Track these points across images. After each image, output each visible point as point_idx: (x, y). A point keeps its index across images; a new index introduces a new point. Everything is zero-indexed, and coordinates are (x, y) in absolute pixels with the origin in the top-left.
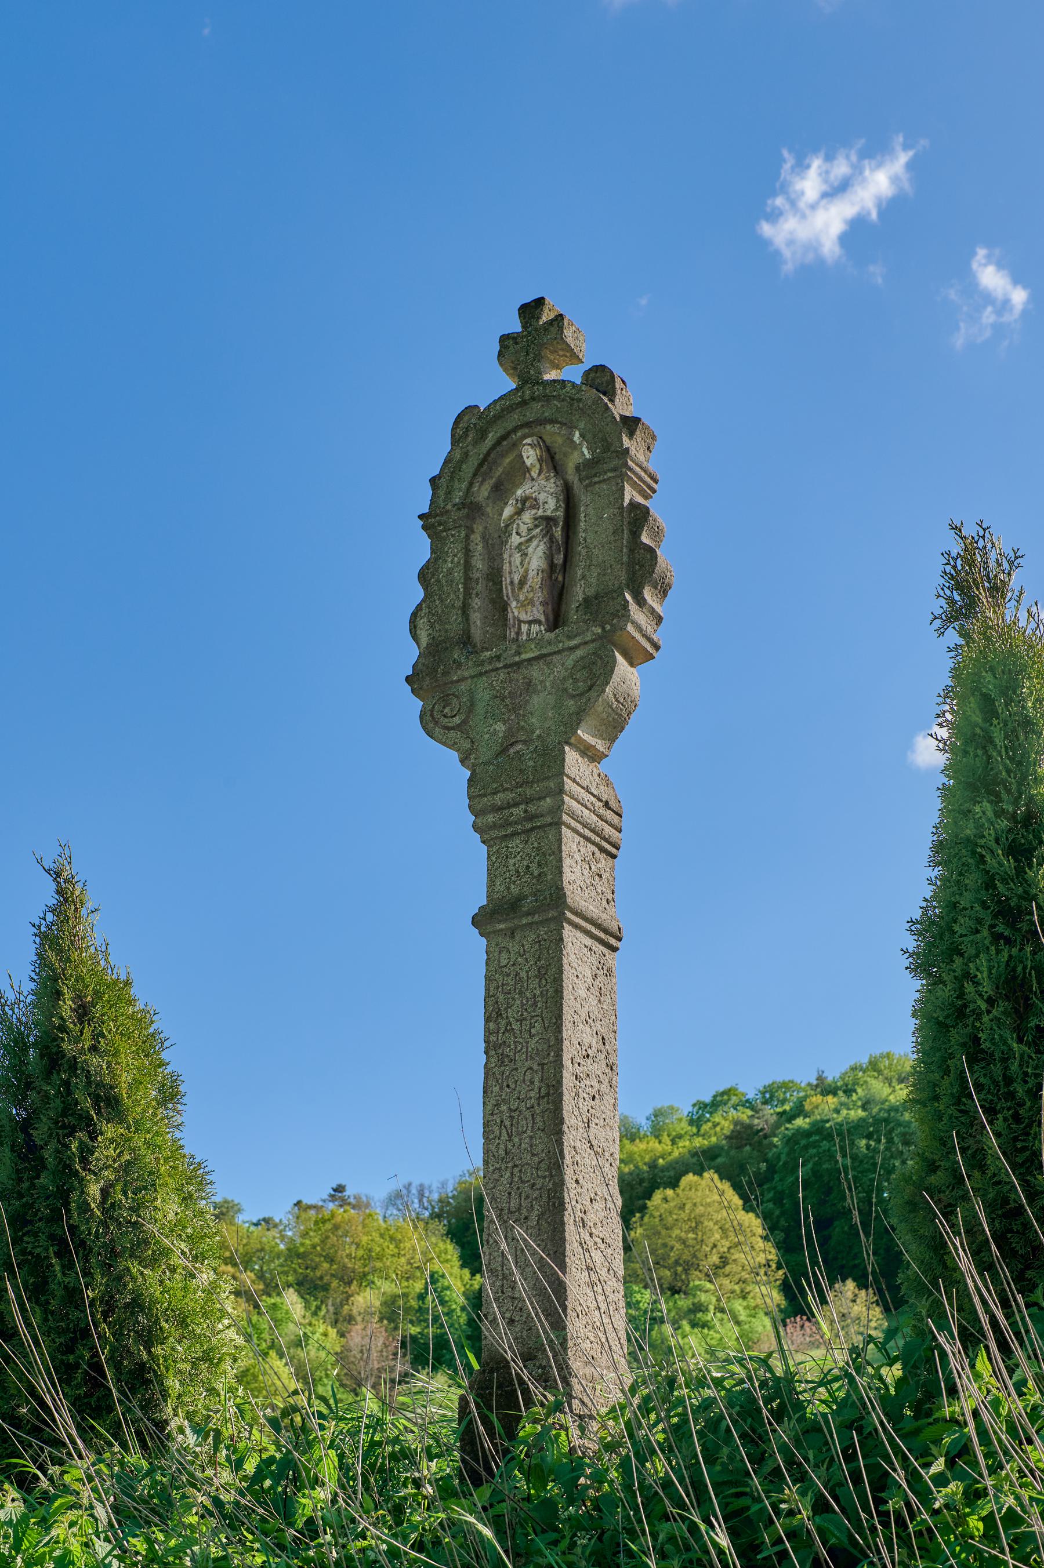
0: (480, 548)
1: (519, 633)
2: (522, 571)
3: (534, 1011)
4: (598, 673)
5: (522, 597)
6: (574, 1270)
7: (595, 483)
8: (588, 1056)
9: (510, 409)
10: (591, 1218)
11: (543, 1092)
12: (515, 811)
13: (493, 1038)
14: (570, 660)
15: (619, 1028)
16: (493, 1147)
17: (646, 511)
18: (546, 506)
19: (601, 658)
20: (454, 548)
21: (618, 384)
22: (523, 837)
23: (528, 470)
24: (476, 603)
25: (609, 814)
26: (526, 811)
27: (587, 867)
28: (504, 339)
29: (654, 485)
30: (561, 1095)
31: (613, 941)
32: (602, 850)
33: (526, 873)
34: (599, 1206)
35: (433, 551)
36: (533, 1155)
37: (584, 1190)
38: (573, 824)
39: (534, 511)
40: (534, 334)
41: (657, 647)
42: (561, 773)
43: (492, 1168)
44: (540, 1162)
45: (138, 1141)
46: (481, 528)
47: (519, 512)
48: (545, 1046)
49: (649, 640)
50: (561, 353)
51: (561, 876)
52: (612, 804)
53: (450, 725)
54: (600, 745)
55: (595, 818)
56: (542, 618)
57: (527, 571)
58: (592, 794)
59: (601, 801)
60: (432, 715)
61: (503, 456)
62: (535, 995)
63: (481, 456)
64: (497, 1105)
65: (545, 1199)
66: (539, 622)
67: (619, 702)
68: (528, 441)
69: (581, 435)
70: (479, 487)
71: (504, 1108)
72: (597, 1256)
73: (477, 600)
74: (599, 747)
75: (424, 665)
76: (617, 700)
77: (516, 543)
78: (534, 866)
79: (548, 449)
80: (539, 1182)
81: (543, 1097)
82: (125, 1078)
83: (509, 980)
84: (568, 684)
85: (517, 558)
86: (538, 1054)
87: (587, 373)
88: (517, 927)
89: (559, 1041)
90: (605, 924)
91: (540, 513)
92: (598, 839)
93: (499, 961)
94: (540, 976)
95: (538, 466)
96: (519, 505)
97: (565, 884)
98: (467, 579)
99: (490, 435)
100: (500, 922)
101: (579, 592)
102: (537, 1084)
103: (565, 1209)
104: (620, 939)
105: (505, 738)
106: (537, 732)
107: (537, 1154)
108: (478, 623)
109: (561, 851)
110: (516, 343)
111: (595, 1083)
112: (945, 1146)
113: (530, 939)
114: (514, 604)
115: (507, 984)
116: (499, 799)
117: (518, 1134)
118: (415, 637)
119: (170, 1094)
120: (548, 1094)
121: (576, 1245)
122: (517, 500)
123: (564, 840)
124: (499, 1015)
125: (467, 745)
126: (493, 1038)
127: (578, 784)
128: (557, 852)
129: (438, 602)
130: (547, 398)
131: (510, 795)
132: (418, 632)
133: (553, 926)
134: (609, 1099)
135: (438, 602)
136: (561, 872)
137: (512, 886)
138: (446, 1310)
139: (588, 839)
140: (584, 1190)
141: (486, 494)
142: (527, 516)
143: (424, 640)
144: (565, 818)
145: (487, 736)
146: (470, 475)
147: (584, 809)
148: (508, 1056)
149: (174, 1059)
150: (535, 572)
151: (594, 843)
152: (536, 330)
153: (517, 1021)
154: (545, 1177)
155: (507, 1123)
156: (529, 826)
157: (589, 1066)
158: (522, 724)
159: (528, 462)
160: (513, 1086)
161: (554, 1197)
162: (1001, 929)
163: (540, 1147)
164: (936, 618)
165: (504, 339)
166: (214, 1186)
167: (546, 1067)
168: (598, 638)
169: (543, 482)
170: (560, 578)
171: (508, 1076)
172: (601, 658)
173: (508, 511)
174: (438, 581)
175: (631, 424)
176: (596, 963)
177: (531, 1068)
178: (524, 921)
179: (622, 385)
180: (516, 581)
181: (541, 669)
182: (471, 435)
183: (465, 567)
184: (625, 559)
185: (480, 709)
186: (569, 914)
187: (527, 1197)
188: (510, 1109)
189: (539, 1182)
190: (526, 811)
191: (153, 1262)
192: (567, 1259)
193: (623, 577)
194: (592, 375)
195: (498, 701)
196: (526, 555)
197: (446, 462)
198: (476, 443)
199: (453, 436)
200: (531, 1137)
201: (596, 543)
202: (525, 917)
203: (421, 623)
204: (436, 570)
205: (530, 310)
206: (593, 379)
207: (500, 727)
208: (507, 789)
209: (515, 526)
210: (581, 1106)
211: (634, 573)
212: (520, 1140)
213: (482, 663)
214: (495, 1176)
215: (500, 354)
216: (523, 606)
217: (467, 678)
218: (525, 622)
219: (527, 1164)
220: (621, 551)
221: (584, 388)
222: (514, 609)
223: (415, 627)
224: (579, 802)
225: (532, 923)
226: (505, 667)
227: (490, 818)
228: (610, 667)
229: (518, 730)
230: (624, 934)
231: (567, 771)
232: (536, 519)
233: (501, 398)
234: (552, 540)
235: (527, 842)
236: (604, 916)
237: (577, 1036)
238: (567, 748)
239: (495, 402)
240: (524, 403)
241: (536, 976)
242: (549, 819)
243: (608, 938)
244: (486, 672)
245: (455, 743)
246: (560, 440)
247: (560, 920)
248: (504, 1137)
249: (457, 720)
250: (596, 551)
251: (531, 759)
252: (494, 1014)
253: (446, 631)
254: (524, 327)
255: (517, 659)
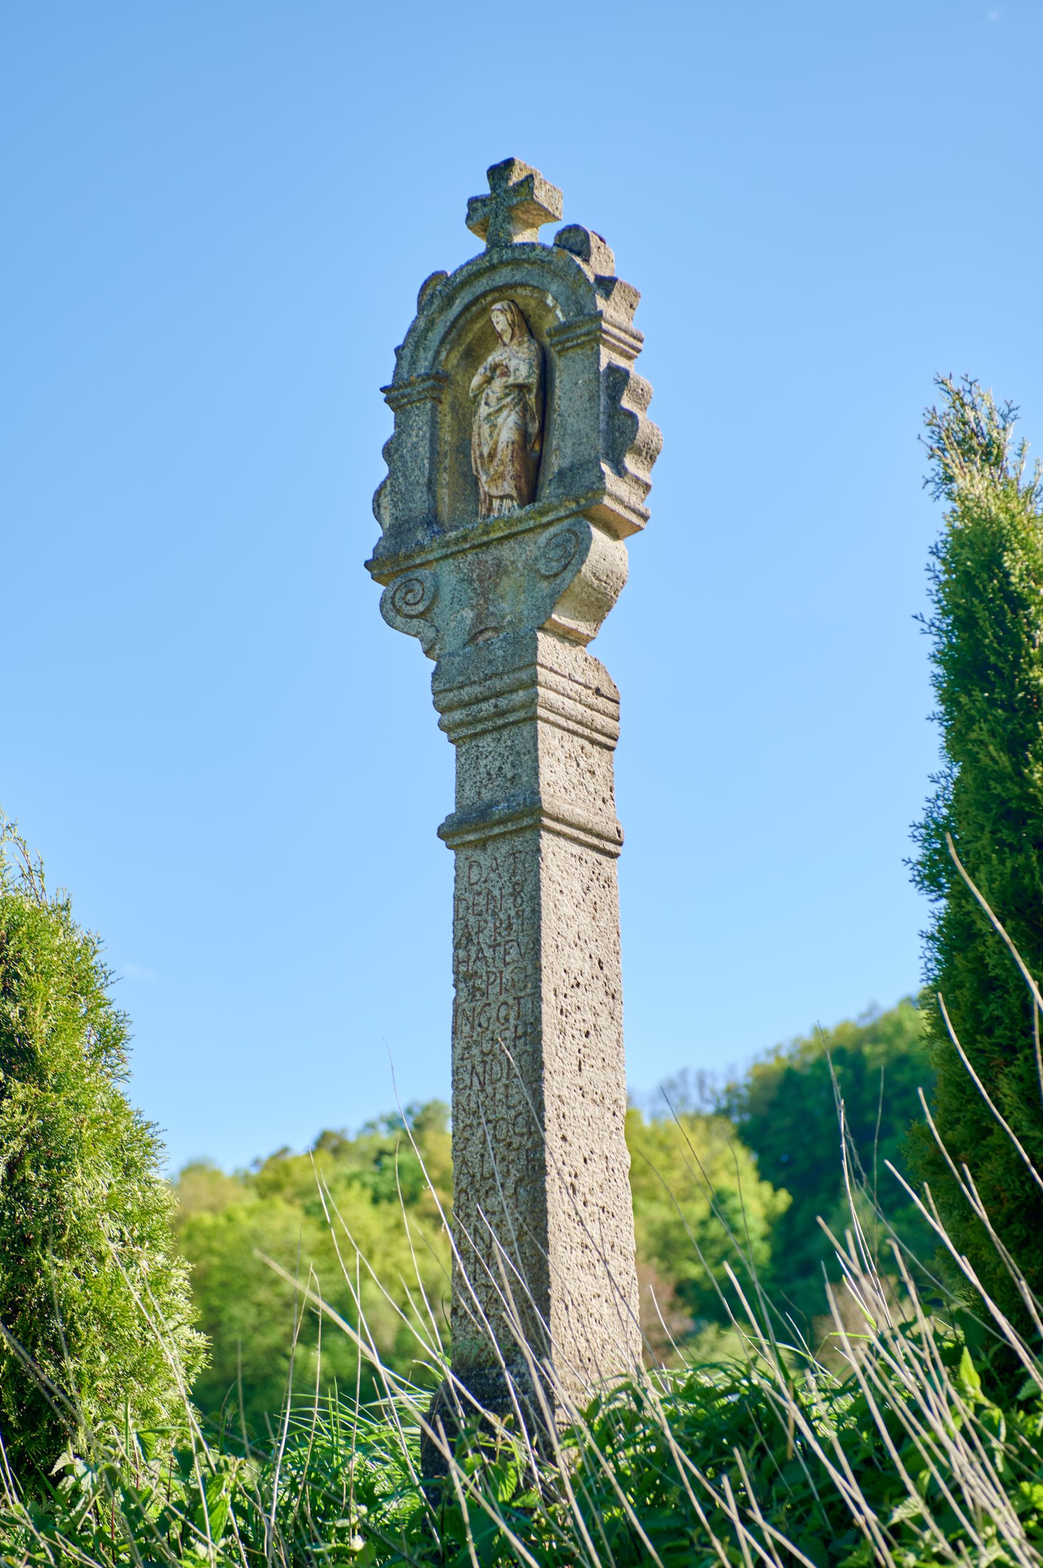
0: (448, 419)
1: (490, 509)
2: (491, 443)
3: (509, 935)
4: (573, 551)
5: (492, 471)
6: (561, 1249)
7: (568, 348)
8: (578, 985)
9: (478, 274)
10: (584, 1184)
11: (520, 1031)
12: (484, 706)
13: (463, 968)
14: (543, 538)
15: (622, 947)
16: (463, 1100)
17: (626, 374)
18: (518, 373)
19: (576, 535)
20: (420, 421)
21: (594, 241)
22: (496, 735)
23: (500, 336)
24: (445, 478)
25: (601, 703)
26: (496, 706)
27: (574, 764)
28: (472, 202)
29: (638, 345)
30: (539, 1035)
31: (611, 847)
32: (593, 742)
33: (498, 776)
34: (597, 1166)
35: (397, 425)
36: (509, 1108)
37: (575, 1148)
38: (552, 717)
39: (504, 379)
40: (504, 198)
41: (645, 518)
42: (534, 663)
43: (461, 1125)
44: (516, 1117)
45: (57, 1101)
46: (449, 398)
47: (489, 381)
48: (522, 976)
49: (634, 511)
50: (535, 212)
51: (537, 778)
52: (604, 690)
53: (412, 613)
54: (583, 628)
55: (581, 708)
56: (514, 494)
57: (496, 443)
58: (576, 682)
59: (590, 688)
60: (393, 603)
61: (472, 321)
62: (509, 916)
63: (449, 323)
64: (468, 1048)
65: (523, 1162)
66: (511, 497)
67: (600, 580)
68: (498, 306)
69: (555, 298)
70: (448, 355)
71: (475, 1051)
72: (593, 1228)
73: (445, 475)
74: (580, 630)
75: (384, 547)
76: (598, 579)
77: (485, 414)
78: (507, 768)
79: (522, 313)
80: (516, 1141)
81: (520, 1038)
82: (41, 1026)
83: (481, 900)
84: (541, 565)
85: (486, 429)
86: (514, 986)
87: (560, 234)
88: (489, 838)
89: (538, 969)
90: (598, 828)
91: (511, 380)
92: (587, 732)
93: (469, 878)
94: (515, 895)
95: (510, 331)
96: (488, 373)
97: (543, 788)
98: (434, 452)
99: (457, 301)
100: (468, 832)
101: (555, 463)
102: (512, 1022)
103: (546, 1174)
104: (620, 844)
105: (473, 626)
106: (509, 618)
107: (514, 1107)
108: (446, 500)
109: (536, 750)
110: (485, 205)
111: (589, 1016)
112: (964, 1093)
113: (503, 851)
114: (484, 478)
115: (478, 905)
116: (466, 693)
117: (492, 1083)
118: (378, 517)
119: (110, 1040)
120: (525, 1034)
121: (562, 1217)
122: (486, 369)
123: (540, 736)
124: (469, 940)
125: (431, 634)
126: (463, 968)
127: (556, 672)
128: (532, 750)
129: (401, 479)
130: (516, 263)
131: (477, 689)
132: (382, 511)
133: (528, 835)
134: (609, 1035)
135: (401, 479)
136: (537, 774)
137: (483, 791)
138: (739, 1241)
139: (574, 733)
140: (575, 1148)
141: (455, 362)
142: (498, 384)
143: (387, 520)
144: (541, 712)
145: (453, 624)
146: (437, 343)
147: (566, 700)
148: (479, 989)
149: (118, 997)
150: (505, 444)
151: (582, 736)
152: (505, 191)
153: (490, 947)
154: (522, 1135)
155: (480, 1069)
156: (500, 722)
157: (580, 996)
158: (492, 609)
159: (499, 328)
160: (485, 1025)
161: (533, 1159)
162: (1005, 834)
163: (517, 1097)
164: (927, 482)
165: (472, 202)
166: (165, 1150)
167: (522, 1001)
168: (573, 514)
169: (515, 347)
170: (537, 447)
171: (480, 1014)
172: (576, 535)
173: (476, 381)
174: (402, 456)
175: (606, 284)
176: (587, 873)
177: (505, 1003)
178: (496, 831)
179: (600, 243)
180: (486, 454)
181: (512, 549)
182: (437, 302)
183: (431, 440)
184: (602, 426)
185: (446, 594)
186: (546, 821)
187: (503, 1159)
188: (482, 1053)
189: (516, 1141)
190: (496, 706)
191: (69, 1251)
192: (550, 1236)
193: (601, 445)
194: (566, 235)
195: (465, 585)
196: (495, 426)
197: (411, 331)
198: (442, 310)
199: (419, 303)
200: (507, 1086)
201: (570, 411)
202: (497, 826)
203: (385, 501)
204: (400, 445)
205: (499, 172)
206: (567, 239)
207: (469, 614)
208: (475, 682)
209: (484, 395)
210: (568, 1045)
211: (614, 441)
212: (494, 1089)
213: (447, 545)
214: (466, 1135)
215: (469, 217)
216: (493, 480)
217: (431, 561)
218: (496, 497)
219: (503, 1119)
220: (598, 418)
221: (555, 250)
222: (485, 486)
223: (379, 506)
224: (558, 693)
225: (505, 833)
226: (473, 547)
227: (458, 715)
228: (584, 545)
229: (487, 616)
230: (625, 837)
231: (540, 659)
232: (506, 387)
233: (468, 263)
234: (525, 408)
235: (499, 740)
236: (597, 819)
237: (559, 962)
238: (540, 635)
239: (462, 268)
240: (493, 268)
241: (511, 895)
242: (522, 714)
243: (605, 845)
244: (452, 554)
245: (419, 633)
246: (533, 303)
247: (537, 827)
248: (477, 1086)
249: (420, 608)
250: (571, 420)
251: (501, 647)
252: (464, 939)
253: (410, 510)
254: (493, 188)
255: (485, 539)
